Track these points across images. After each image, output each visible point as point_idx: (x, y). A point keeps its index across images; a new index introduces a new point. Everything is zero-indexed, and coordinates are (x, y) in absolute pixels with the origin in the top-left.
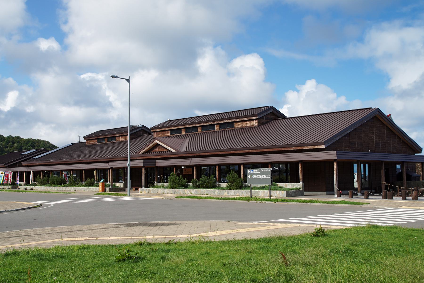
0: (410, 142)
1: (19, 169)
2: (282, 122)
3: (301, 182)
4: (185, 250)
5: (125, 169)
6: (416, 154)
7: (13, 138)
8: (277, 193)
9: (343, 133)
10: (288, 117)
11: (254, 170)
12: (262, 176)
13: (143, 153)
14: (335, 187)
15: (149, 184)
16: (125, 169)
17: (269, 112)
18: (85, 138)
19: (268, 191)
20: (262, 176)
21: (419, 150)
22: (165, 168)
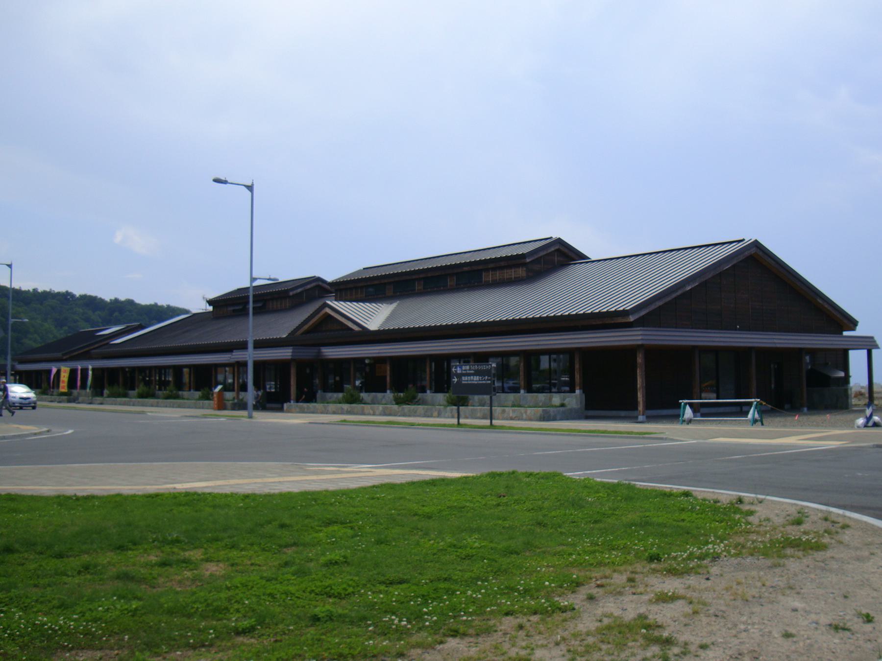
0: (830, 308)
1: (79, 366)
2: (576, 271)
3: (578, 392)
4: (848, 630)
5: (244, 364)
6: (845, 333)
7: (122, 302)
8: (526, 412)
9: (676, 291)
10: (593, 259)
11: (464, 368)
12: (476, 379)
13: (303, 334)
14: (90, 373)
15: (307, 396)
16: (244, 364)
17: (553, 249)
18: (210, 302)
19: (455, 408)
20: (476, 379)
21: (852, 324)
22: (342, 365)
